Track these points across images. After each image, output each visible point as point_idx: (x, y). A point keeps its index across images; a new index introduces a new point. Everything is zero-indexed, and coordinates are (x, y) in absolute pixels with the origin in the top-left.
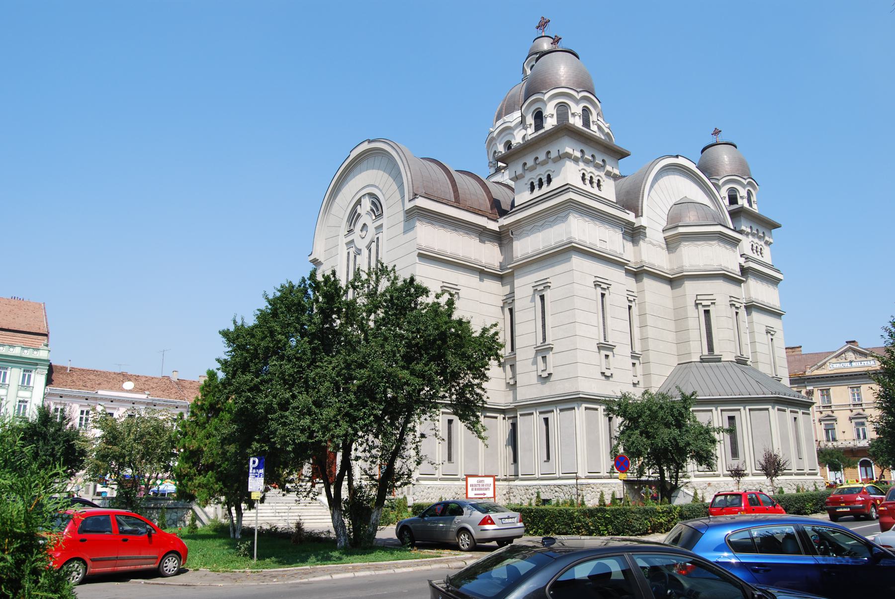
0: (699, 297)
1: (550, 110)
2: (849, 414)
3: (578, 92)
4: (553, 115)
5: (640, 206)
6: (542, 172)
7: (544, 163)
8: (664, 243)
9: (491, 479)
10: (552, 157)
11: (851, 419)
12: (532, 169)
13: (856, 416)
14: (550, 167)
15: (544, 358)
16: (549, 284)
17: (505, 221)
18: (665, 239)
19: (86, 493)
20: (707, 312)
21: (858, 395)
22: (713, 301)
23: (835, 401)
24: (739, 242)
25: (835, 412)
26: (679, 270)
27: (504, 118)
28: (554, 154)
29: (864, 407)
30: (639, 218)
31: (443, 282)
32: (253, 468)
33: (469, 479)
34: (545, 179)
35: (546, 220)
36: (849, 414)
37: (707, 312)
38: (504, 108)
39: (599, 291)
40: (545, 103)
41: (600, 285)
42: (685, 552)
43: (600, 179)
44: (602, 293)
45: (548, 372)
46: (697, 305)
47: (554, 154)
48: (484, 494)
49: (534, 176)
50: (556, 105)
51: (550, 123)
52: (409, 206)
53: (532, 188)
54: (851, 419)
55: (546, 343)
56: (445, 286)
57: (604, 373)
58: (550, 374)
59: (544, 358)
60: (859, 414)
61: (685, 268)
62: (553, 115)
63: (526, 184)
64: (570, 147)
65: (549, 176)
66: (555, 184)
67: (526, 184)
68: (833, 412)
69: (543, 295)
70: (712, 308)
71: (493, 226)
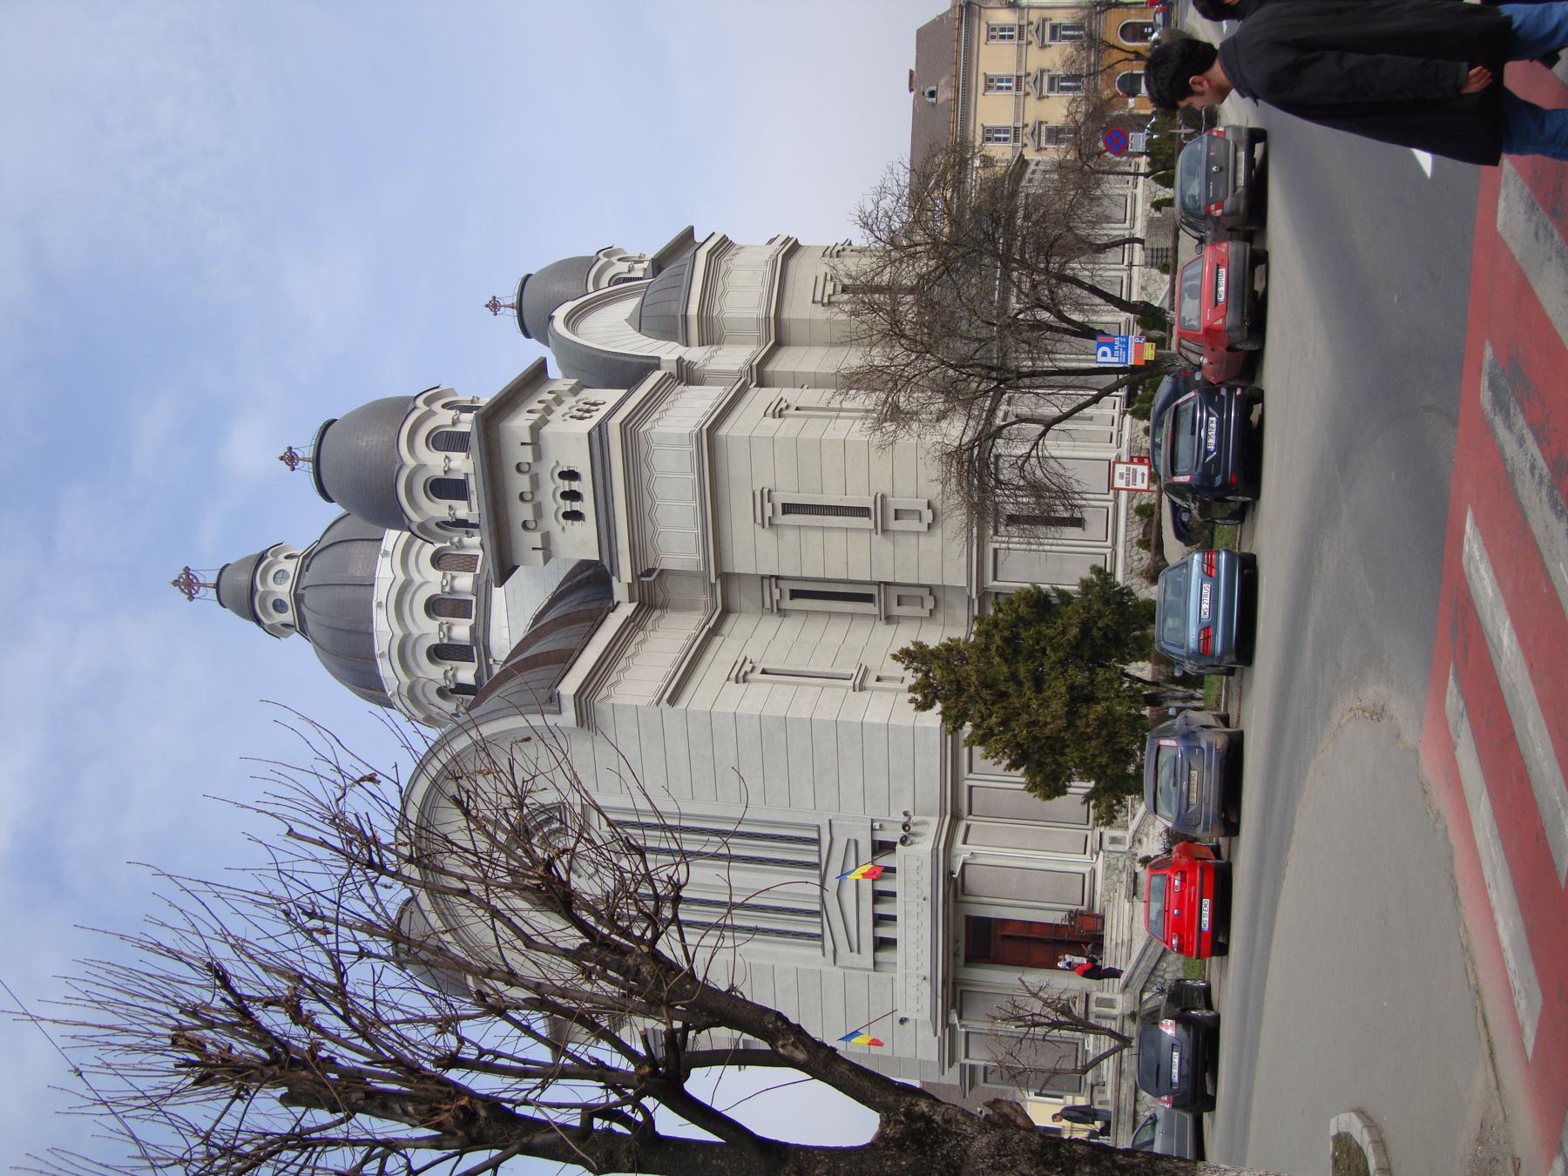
0: (818, 298)
1: (436, 463)
2: (1033, 49)
3: (415, 408)
4: (447, 457)
5: (640, 360)
6: (552, 487)
7: (535, 482)
8: (708, 347)
9: (1117, 466)
10: (530, 460)
11: (1043, 46)
12: (538, 511)
13: (1040, 36)
14: (547, 471)
15: (898, 514)
16: (766, 491)
17: (620, 590)
18: (701, 344)
19: (1119, 977)
20: (788, 508)
21: (1001, 80)
22: (829, 277)
23: (1006, 120)
24: (727, 239)
25: (1026, 122)
26: (762, 325)
27: (389, 693)
28: (526, 455)
29: (1023, 73)
30: (662, 365)
31: (728, 679)
32: (1113, 356)
33: (1116, 485)
34: (565, 485)
35: (644, 487)
36: (1033, 49)
37: (788, 508)
38: (368, 691)
39: (757, 675)
40: (421, 467)
41: (746, 673)
42: (1239, 167)
43: (560, 514)
44: (784, 513)
45: (924, 508)
46: (830, 303)
47: (526, 455)
48: (1143, 474)
49: (554, 506)
50: (428, 448)
51: (462, 464)
52: (569, 716)
53: (574, 516)
54: (1043, 46)
55: (872, 507)
56: (774, 411)
57: (931, 610)
58: (929, 505)
59: (898, 514)
60: (1037, 31)
61: (762, 315)
62: (447, 457)
63: (563, 529)
64: (519, 424)
65: (563, 475)
66: (583, 465)
67: (563, 529)
68: (1026, 126)
69: (783, 505)
70: (780, 499)
71: (627, 609)
